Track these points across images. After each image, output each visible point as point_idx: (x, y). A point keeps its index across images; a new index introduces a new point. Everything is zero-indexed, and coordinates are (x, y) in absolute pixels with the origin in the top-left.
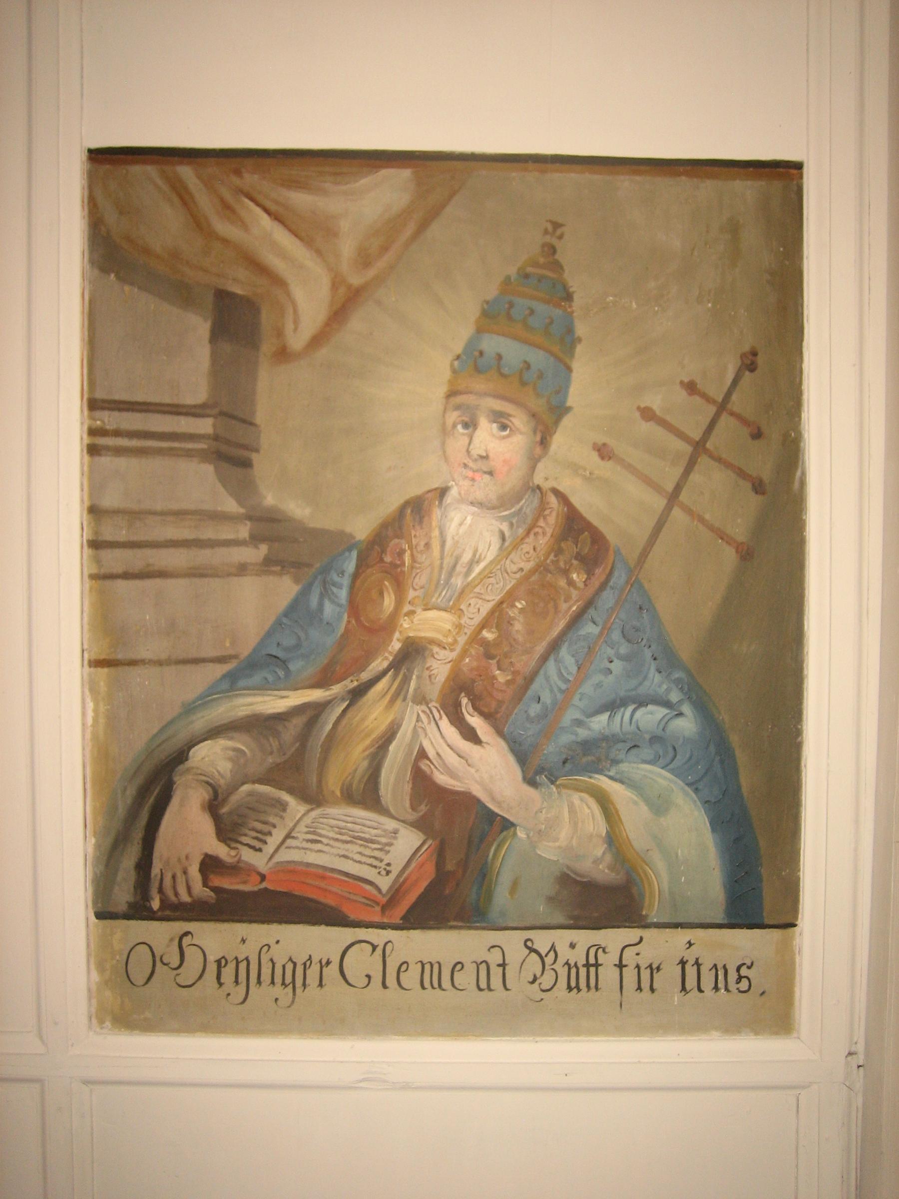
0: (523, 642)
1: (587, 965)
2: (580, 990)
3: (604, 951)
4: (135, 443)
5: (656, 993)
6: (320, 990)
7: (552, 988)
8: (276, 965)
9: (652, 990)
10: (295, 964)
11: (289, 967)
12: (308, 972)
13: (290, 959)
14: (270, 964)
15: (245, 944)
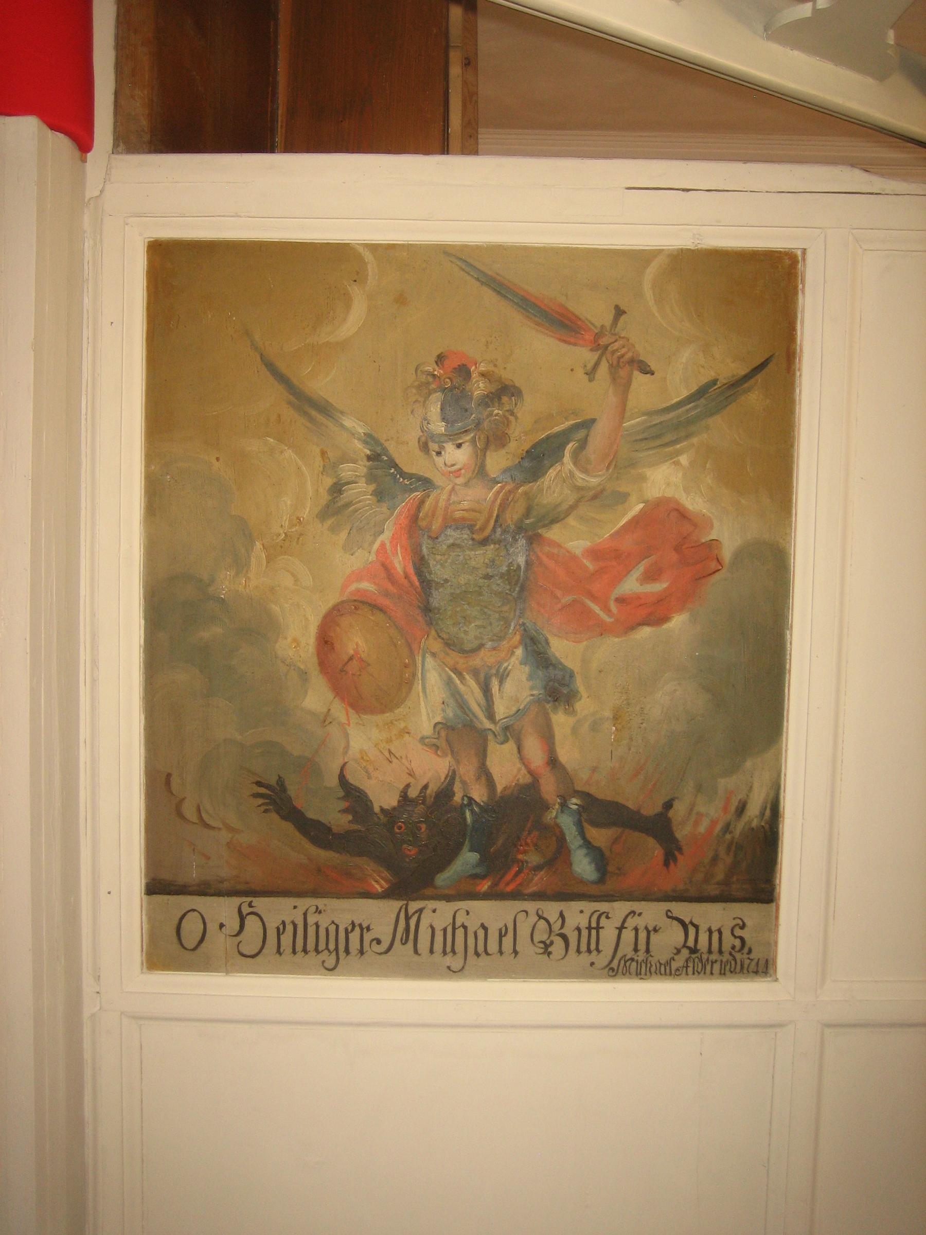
0: (423, 517)
1: (589, 928)
2: (503, 953)
3: (607, 917)
4: (834, 114)
5: (504, 955)
6: (453, 956)
7: (238, 946)
8: (489, 931)
9: (516, 952)
10: (337, 926)
11: (332, 928)
12: (282, 937)
13: (333, 922)
14: (430, 930)
15: (559, 911)
